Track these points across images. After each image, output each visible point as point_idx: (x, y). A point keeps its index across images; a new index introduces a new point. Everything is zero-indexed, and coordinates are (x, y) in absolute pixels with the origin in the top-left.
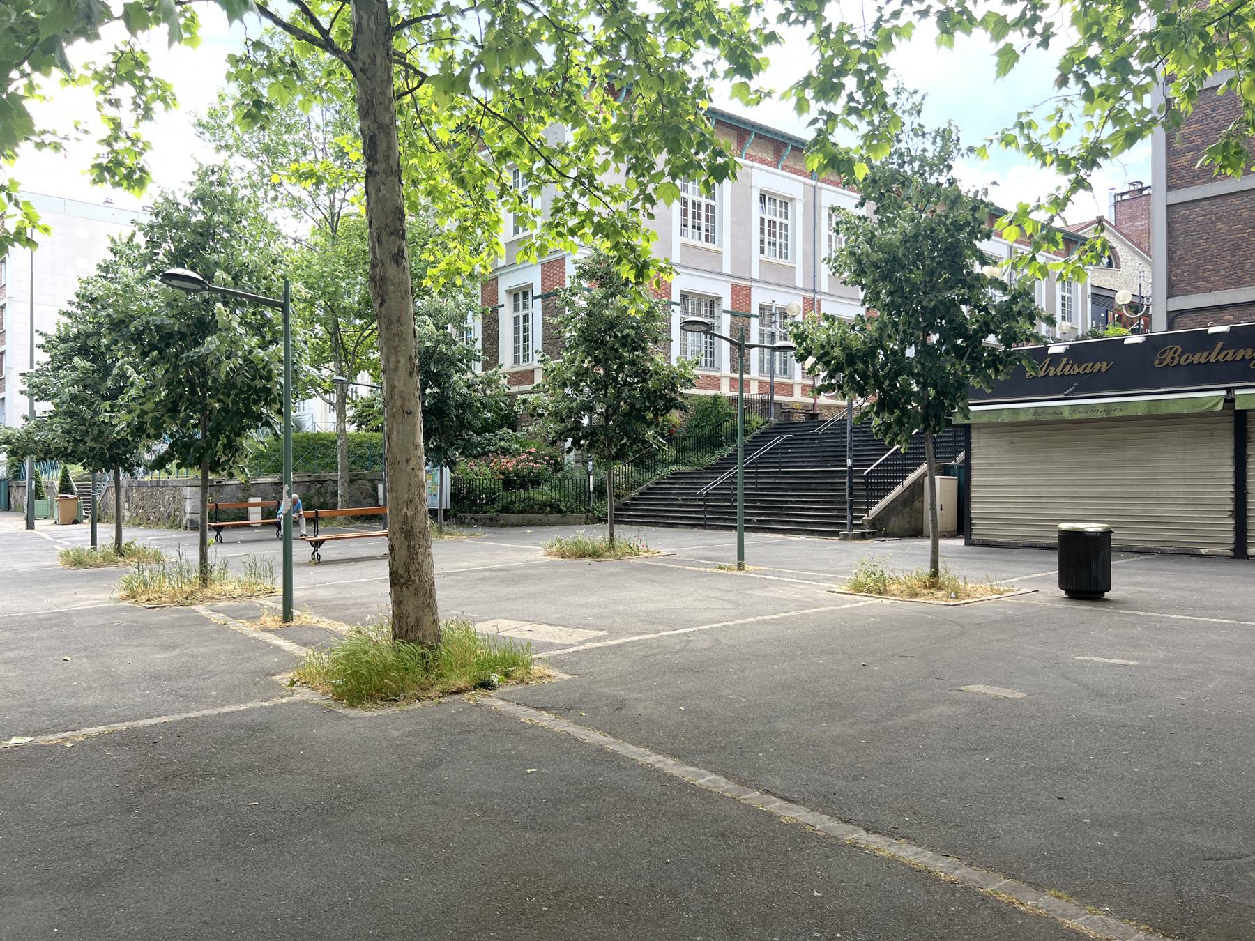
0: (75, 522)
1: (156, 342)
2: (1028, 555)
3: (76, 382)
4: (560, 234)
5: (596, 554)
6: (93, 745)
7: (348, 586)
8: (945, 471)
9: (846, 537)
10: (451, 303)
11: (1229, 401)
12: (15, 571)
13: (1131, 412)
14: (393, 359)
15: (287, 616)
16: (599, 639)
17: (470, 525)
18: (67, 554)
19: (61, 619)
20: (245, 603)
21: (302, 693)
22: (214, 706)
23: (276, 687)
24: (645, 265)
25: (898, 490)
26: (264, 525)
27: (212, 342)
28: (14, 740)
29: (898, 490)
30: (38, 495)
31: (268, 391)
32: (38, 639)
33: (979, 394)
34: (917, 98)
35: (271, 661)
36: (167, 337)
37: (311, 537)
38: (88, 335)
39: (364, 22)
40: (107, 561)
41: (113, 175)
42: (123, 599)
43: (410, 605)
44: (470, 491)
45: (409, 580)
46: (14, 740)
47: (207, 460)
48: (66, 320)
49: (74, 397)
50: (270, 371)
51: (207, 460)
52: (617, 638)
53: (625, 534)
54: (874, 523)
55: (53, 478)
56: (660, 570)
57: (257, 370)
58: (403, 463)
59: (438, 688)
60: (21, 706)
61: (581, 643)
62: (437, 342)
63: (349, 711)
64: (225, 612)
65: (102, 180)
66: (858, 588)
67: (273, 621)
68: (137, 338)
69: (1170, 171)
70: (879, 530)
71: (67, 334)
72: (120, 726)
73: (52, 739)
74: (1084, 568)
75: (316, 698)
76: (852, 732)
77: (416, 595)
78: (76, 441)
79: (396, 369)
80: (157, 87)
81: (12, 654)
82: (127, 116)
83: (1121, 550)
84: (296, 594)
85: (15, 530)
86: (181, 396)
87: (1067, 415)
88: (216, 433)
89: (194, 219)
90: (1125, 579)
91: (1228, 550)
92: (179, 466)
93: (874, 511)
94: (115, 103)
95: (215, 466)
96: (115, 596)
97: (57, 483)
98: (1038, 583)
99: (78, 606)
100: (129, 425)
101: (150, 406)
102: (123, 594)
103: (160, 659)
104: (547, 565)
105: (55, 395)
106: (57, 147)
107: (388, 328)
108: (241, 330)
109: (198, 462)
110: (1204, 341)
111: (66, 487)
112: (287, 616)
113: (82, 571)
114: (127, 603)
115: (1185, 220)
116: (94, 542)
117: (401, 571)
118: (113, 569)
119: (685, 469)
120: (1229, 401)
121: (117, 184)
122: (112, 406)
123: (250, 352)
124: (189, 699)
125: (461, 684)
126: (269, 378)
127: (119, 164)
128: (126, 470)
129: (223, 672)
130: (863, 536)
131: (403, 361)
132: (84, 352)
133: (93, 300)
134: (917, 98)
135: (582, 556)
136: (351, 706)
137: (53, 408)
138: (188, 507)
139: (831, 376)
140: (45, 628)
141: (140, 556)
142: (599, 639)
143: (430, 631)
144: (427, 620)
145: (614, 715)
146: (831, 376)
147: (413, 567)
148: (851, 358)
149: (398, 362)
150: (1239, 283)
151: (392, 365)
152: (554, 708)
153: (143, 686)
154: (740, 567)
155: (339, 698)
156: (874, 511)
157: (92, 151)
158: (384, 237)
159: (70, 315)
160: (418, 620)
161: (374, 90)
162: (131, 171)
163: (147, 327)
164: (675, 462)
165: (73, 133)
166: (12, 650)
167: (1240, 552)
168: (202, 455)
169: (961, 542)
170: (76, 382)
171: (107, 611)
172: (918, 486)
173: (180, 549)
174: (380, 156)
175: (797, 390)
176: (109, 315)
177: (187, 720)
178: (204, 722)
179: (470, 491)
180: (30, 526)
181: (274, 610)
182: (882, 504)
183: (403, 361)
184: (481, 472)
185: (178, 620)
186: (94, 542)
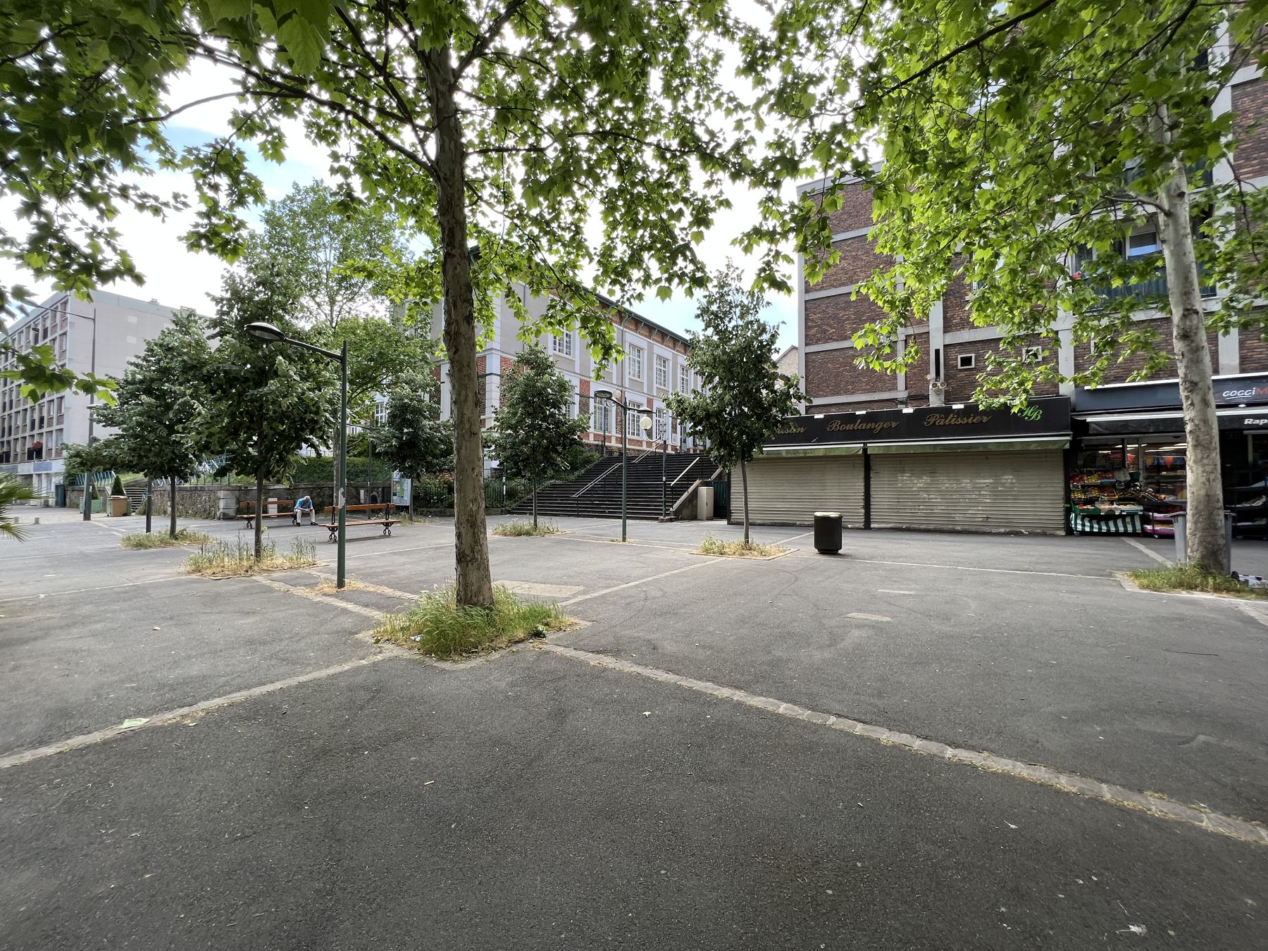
0: (125, 515)
1: (219, 382)
2: (764, 529)
3: (140, 414)
4: (551, 324)
5: (528, 534)
6: (215, 722)
7: (413, 558)
8: (707, 484)
9: (662, 521)
10: (420, 376)
11: (865, 450)
12: (82, 553)
13: (817, 454)
14: (463, 393)
15: (341, 584)
16: (579, 593)
17: (426, 515)
18: (129, 539)
19: (139, 592)
20: (295, 573)
21: (390, 651)
22: (319, 668)
23: (360, 644)
24: (610, 347)
25: (686, 495)
26: (279, 517)
27: (273, 384)
28: (127, 724)
29: (686, 495)
30: (93, 496)
31: (316, 422)
32: (121, 610)
33: (769, 442)
34: (738, 272)
35: (347, 622)
36: (231, 379)
37: (329, 525)
38: (152, 380)
39: (447, 147)
40: (163, 542)
41: (210, 242)
42: (189, 573)
43: (473, 577)
44: (426, 494)
45: (470, 557)
46: (127, 724)
47: (263, 469)
48: (133, 368)
49: (139, 424)
50: (318, 408)
51: (263, 469)
52: (594, 591)
53: (542, 521)
54: (675, 513)
55: (107, 485)
56: (575, 543)
57: (308, 406)
58: (470, 471)
59: (505, 638)
60: (123, 681)
61: (574, 596)
62: (411, 400)
63: (447, 665)
64: (285, 581)
65: (199, 246)
66: (707, 551)
67: (330, 588)
68: (207, 379)
69: (806, 336)
70: (678, 517)
71: (134, 379)
72: (238, 697)
73: (169, 717)
74: (828, 537)
75: (406, 655)
76: (827, 655)
77: (478, 569)
78: (140, 457)
79: (466, 401)
80: (249, 183)
81: (99, 626)
82: (224, 200)
83: (809, 526)
84: (348, 564)
85: (73, 521)
86: (241, 424)
87: (784, 455)
88: (270, 449)
89: (256, 298)
90: (849, 543)
91: (861, 525)
92: (238, 474)
93: (676, 506)
94: (215, 187)
95: (268, 474)
96: (182, 569)
97: (109, 490)
98: (803, 545)
99: (148, 580)
100: (196, 443)
101: (216, 429)
102: (189, 568)
103: (247, 625)
104: (499, 541)
105: (123, 423)
106: (156, 211)
107: (460, 370)
108: (296, 377)
109: (255, 472)
110: (853, 418)
111: (117, 489)
112: (341, 584)
113: (143, 551)
114: (193, 576)
115: (814, 361)
116: (148, 529)
117: (468, 552)
118: (169, 549)
119: (558, 482)
120: (865, 450)
121: (212, 251)
122: (184, 429)
123: (303, 394)
124: (294, 662)
125: (521, 635)
126: (317, 413)
127: (217, 234)
128: (181, 478)
129: (309, 634)
130: (671, 520)
131: (471, 395)
132: (148, 392)
133: (170, 349)
134: (738, 272)
135: (519, 535)
136: (441, 659)
137: (120, 432)
138: (222, 504)
139: (695, 426)
140: (125, 600)
141: (193, 539)
142: (584, 593)
143: (487, 595)
144: (486, 588)
145: (651, 653)
146: (695, 426)
147: (477, 548)
148: (708, 416)
149: (467, 396)
150: (838, 394)
151: (462, 398)
152: (610, 651)
153: (242, 652)
154: (624, 540)
155: (428, 653)
156: (676, 506)
157: (188, 219)
158: (459, 303)
159: (137, 365)
160: (480, 587)
161: (453, 195)
162: (227, 242)
163: (217, 371)
164: (552, 478)
165: (172, 202)
166: (96, 622)
167: (867, 527)
168: (259, 467)
169: (724, 522)
170: (140, 414)
171: (177, 584)
172: (695, 492)
173: (238, 535)
174: (457, 245)
175: (613, 440)
176: (184, 361)
177: (301, 685)
178: (318, 686)
179: (426, 494)
180: (87, 517)
181: (332, 581)
182: (679, 502)
183: (471, 395)
184: (431, 482)
185: (245, 588)
186: (148, 529)
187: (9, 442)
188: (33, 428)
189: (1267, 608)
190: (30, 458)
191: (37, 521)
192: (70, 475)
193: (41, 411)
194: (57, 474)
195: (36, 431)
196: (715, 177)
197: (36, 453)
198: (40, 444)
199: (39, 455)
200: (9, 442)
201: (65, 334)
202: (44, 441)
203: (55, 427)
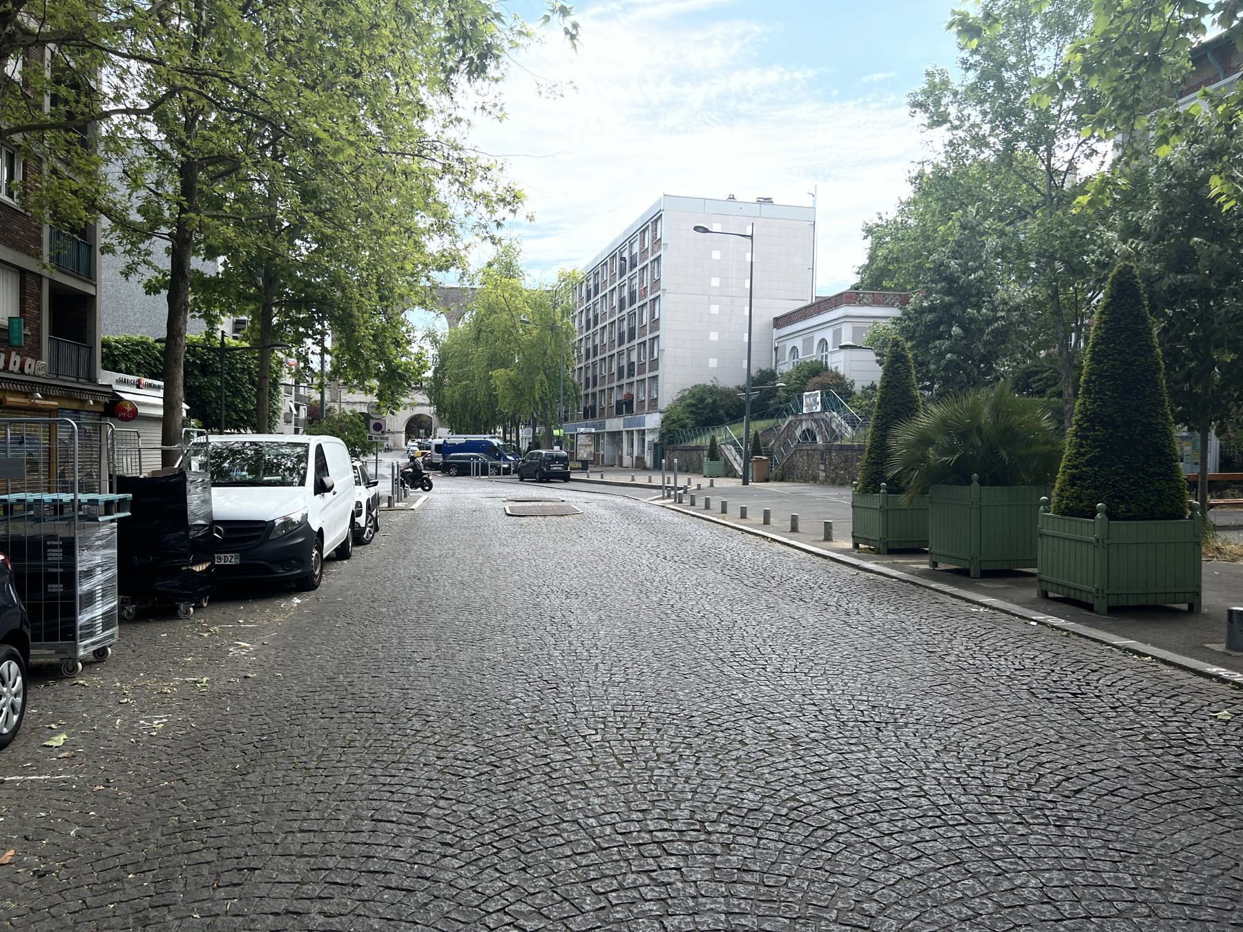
85: (729, 485)
187: (594, 395)
188: (621, 376)
189: (5, 474)
190: (619, 412)
191: (712, 485)
192: (669, 431)
193: (594, 368)
194: (652, 431)
195: (625, 381)
196: (965, 113)
197: (626, 406)
198: (630, 396)
199: (630, 410)
200: (594, 395)
201: (658, 259)
202: (634, 392)
203: (648, 375)
